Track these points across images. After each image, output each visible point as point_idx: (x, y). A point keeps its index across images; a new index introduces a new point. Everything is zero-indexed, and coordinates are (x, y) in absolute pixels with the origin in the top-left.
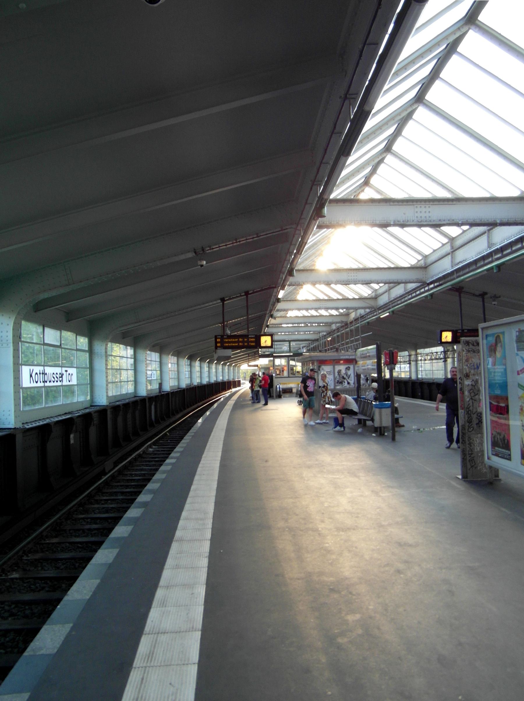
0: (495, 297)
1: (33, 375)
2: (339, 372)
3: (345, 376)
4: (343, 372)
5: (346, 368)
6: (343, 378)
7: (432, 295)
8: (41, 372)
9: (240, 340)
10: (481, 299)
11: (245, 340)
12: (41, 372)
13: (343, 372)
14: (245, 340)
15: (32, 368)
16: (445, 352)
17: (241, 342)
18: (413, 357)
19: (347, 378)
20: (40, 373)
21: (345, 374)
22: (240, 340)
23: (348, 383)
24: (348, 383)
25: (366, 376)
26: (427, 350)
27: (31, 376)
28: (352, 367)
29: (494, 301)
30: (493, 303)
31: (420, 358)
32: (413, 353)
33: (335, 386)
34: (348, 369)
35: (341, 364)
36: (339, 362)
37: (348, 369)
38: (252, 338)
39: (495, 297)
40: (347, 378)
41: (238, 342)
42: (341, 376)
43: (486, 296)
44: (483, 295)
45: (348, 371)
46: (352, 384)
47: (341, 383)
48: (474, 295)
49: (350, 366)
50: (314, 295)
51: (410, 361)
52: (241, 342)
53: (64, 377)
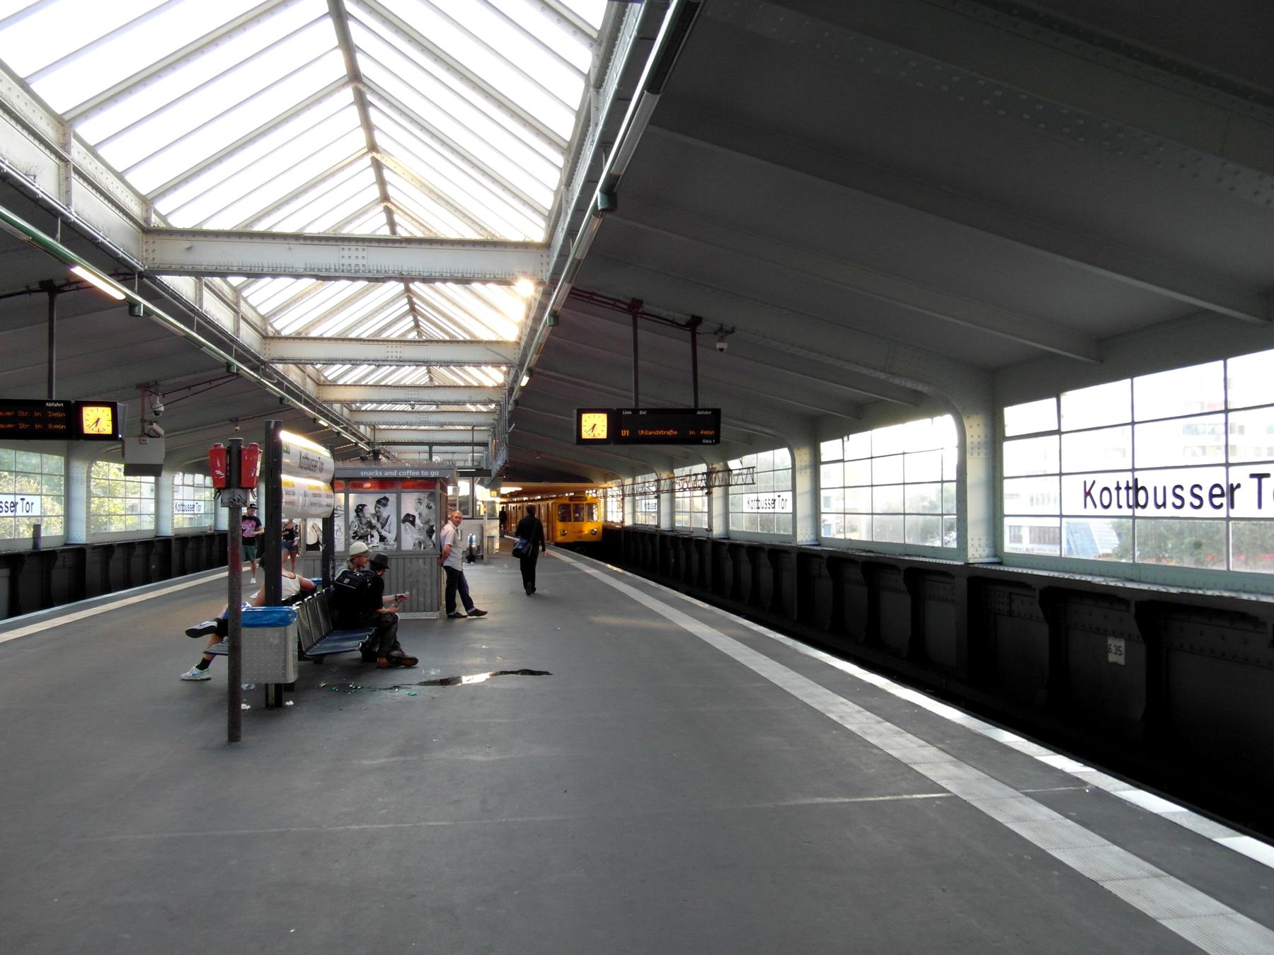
0: (723, 332)
1: (1095, 493)
2: (360, 509)
3: (374, 521)
4: (370, 509)
5: (379, 502)
6: (372, 527)
7: (554, 315)
8: (1123, 485)
9: (21, 413)
10: (688, 335)
11: (37, 414)
12: (1123, 485)
13: (370, 509)
14: (37, 414)
15: (1089, 479)
16: (709, 474)
17: (24, 420)
18: (665, 485)
19: (379, 526)
20: (1118, 488)
21: (374, 515)
22: (21, 413)
23: (382, 539)
24: (382, 539)
25: (427, 522)
26: (687, 470)
27: (1088, 494)
28: (392, 498)
29: (721, 340)
30: (719, 345)
31: (677, 487)
32: (665, 475)
33: (348, 545)
34: (382, 502)
35: (366, 492)
36: (361, 486)
37: (382, 502)
38: (54, 409)
39: (723, 332)
40: (379, 526)
41: (14, 419)
42: (364, 521)
43: (699, 329)
44: (694, 323)
45: (382, 509)
46: (392, 542)
47: (363, 538)
48: (673, 323)
49: (387, 495)
50: (472, 292)
51: (658, 491)
52: (24, 420)
53: (19, 507)
